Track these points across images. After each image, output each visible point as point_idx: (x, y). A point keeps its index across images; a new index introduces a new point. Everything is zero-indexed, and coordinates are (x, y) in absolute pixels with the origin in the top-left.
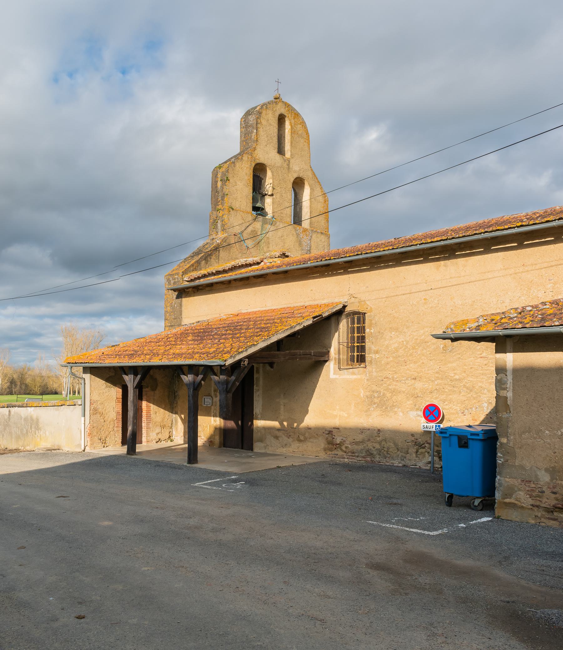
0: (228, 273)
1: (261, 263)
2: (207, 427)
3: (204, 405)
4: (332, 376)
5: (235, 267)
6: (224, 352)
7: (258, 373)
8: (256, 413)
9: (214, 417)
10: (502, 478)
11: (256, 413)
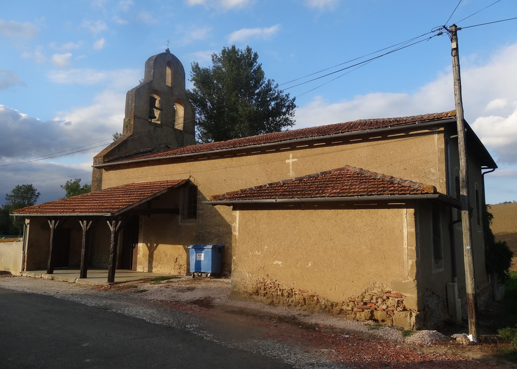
1: (152, 151)
4: (180, 224)
5: (136, 153)
6: (359, 188)
8: (139, 246)
10: (233, 278)
11: (139, 246)
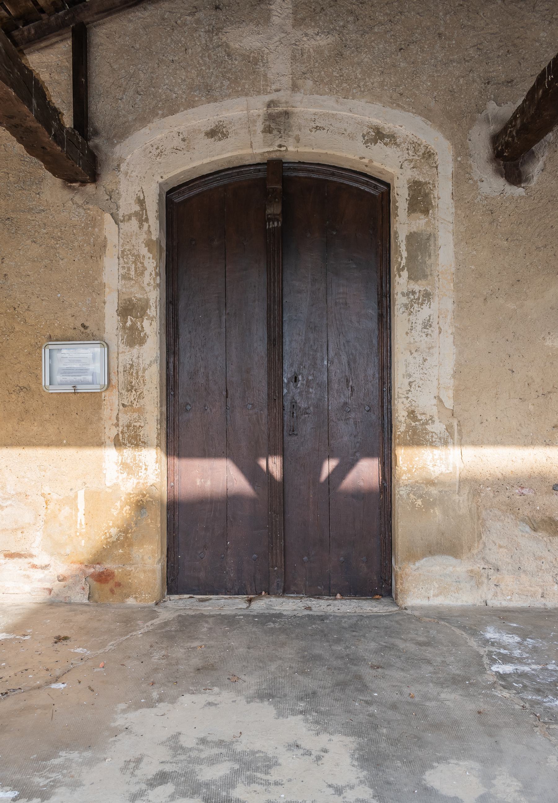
0: (201, 613)
2: (72, 502)
3: (54, 389)
7: (426, 211)
8: (412, 414)
9: (118, 443)
